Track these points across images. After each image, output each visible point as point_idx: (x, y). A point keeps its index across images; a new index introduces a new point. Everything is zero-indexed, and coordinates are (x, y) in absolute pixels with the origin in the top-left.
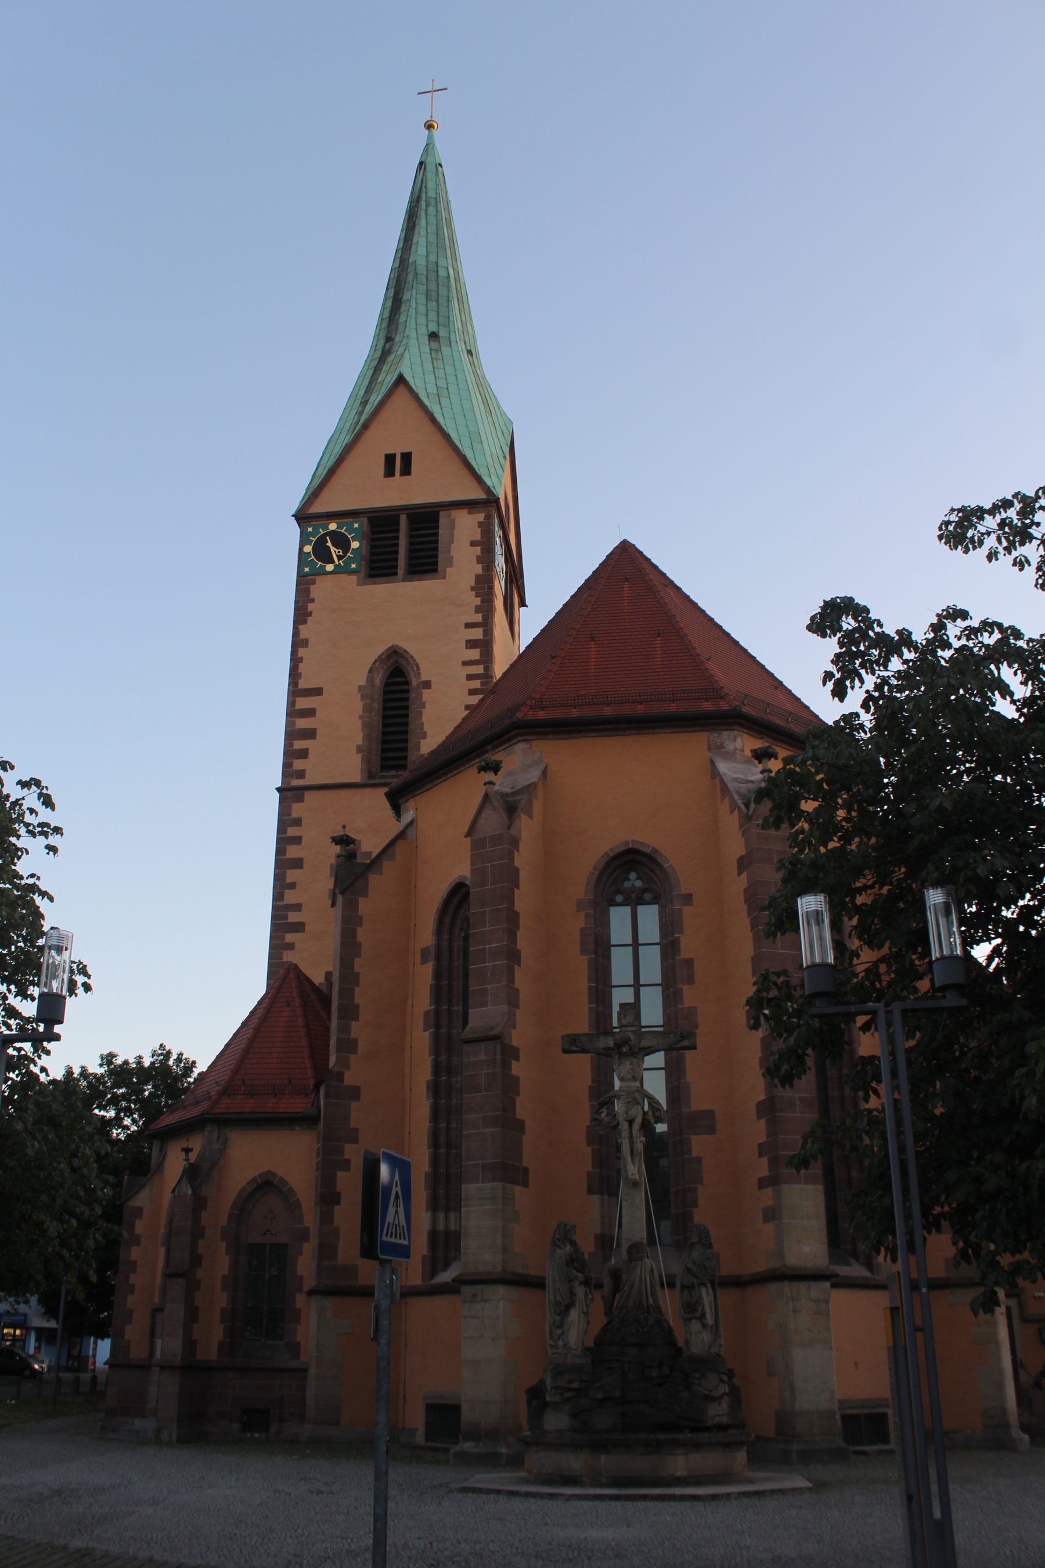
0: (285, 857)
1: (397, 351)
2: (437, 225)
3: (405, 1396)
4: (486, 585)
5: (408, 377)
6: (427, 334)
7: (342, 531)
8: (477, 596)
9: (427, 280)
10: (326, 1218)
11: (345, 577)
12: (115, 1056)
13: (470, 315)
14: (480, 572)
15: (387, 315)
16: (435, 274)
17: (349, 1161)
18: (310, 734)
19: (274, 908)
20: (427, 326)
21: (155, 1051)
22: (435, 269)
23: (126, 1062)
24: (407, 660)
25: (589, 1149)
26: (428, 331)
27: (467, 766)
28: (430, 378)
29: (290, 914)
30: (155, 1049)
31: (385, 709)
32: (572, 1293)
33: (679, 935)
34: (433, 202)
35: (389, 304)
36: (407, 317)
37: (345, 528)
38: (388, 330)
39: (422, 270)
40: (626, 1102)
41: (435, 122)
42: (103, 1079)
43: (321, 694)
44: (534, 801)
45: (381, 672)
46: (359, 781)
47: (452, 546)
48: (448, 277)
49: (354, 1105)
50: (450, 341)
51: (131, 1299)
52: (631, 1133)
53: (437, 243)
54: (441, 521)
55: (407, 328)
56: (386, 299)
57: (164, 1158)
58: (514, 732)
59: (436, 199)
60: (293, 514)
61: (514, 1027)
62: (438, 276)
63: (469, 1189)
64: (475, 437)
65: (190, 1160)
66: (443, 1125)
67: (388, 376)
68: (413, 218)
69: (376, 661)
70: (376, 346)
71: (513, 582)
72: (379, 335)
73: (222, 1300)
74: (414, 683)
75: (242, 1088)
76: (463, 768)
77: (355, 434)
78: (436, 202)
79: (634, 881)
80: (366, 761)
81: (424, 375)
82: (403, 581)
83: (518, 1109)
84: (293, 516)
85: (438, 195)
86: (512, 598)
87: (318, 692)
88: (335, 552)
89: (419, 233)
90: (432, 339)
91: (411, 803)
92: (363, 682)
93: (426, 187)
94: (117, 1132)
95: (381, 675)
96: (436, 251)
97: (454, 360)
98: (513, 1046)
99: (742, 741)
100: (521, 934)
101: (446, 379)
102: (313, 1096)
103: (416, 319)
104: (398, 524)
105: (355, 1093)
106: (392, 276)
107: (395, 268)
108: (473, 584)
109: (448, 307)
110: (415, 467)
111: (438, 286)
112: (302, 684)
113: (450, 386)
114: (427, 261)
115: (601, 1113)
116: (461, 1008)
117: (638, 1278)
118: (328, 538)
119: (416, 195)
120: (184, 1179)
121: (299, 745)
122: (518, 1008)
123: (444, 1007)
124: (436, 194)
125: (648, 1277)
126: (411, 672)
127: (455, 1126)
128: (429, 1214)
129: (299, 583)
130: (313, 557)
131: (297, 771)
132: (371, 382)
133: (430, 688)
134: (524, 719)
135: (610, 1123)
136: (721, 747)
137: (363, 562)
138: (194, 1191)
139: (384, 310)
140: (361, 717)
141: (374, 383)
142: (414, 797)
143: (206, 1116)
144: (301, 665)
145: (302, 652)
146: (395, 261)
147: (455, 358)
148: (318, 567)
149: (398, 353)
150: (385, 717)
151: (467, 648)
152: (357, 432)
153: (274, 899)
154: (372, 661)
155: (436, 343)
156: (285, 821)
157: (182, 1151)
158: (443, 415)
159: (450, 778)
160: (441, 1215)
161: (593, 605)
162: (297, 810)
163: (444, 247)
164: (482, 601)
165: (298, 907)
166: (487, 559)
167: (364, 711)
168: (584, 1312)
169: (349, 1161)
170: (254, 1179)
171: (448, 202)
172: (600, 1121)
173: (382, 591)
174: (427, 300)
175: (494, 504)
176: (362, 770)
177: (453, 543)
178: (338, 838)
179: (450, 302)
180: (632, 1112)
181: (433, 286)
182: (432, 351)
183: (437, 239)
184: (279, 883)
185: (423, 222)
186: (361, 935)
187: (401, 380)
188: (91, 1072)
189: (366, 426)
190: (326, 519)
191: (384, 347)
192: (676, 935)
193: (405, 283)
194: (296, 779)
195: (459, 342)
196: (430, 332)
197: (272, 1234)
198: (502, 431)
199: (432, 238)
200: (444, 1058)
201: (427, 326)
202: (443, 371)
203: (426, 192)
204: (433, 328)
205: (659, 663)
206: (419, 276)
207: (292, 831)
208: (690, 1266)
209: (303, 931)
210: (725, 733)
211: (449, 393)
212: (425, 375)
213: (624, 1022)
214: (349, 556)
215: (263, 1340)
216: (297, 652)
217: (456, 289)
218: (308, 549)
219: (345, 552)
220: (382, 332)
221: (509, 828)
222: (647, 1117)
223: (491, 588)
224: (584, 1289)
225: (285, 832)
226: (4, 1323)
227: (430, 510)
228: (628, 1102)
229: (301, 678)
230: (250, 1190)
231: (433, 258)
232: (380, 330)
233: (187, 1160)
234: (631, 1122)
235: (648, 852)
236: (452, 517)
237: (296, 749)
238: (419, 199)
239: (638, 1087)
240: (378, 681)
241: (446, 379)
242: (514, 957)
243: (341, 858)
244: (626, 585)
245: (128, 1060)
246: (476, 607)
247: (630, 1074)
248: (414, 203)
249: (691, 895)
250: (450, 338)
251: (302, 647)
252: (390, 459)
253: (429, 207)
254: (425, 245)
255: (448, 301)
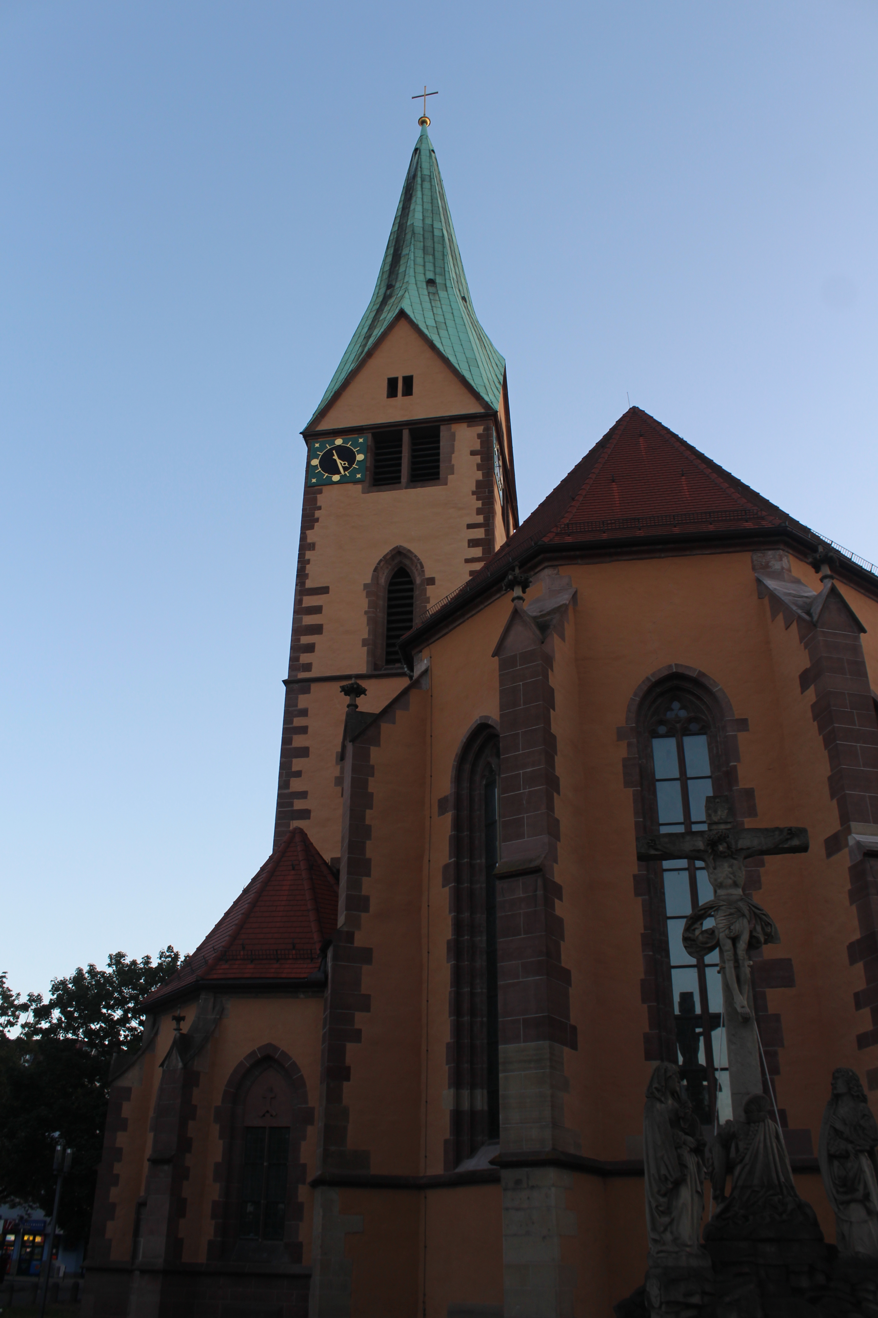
0: (291, 746)
1: (398, 294)
2: (431, 196)
3: (425, 1310)
4: (487, 490)
5: (409, 311)
6: (424, 280)
7: (348, 446)
8: (478, 499)
9: (424, 238)
10: (333, 1096)
11: (350, 486)
12: (123, 956)
13: (463, 271)
14: (481, 478)
15: (387, 268)
16: (431, 234)
17: (359, 1031)
18: (317, 629)
19: (280, 796)
20: (425, 274)
21: (163, 953)
22: (431, 229)
23: (134, 963)
24: (411, 559)
25: (645, 1006)
26: (426, 278)
27: (486, 604)
28: (429, 314)
29: (296, 802)
30: (163, 951)
31: (389, 607)
32: (683, 1166)
33: (736, 764)
34: (427, 179)
35: (389, 259)
36: (406, 267)
37: (350, 443)
38: (389, 280)
39: (419, 230)
40: (728, 913)
41: (428, 118)
42: (112, 979)
43: (327, 592)
44: (566, 624)
45: (386, 572)
46: (365, 672)
47: (453, 455)
48: (443, 236)
49: (365, 968)
50: (446, 287)
51: (114, 1191)
52: (735, 954)
53: (432, 210)
54: (441, 434)
55: (406, 276)
56: (386, 256)
57: (156, 1034)
58: (540, 557)
59: (430, 176)
60: (301, 431)
61: (556, 861)
62: (433, 235)
63: (507, 1050)
64: (472, 362)
65: (181, 1030)
66: (466, 989)
67: (389, 314)
68: (410, 191)
69: (381, 561)
70: (378, 293)
71: (508, 503)
72: (380, 285)
73: (214, 1191)
74: (418, 581)
75: (242, 953)
76: (482, 606)
77: (360, 361)
78: (431, 179)
79: (678, 711)
80: (372, 654)
81: (423, 311)
82: (406, 488)
83: (563, 957)
84: (301, 433)
85: (432, 173)
86: (507, 510)
87: (325, 590)
88: (341, 464)
89: (416, 201)
90: (430, 284)
91: (426, 652)
92: (368, 581)
93: (421, 167)
94: (125, 1033)
95: (385, 574)
96: (431, 216)
97: (450, 302)
98: (554, 882)
99: (788, 561)
100: (558, 760)
101: (443, 315)
102: (320, 960)
103: (414, 268)
104: (401, 440)
105: (366, 955)
106: (392, 238)
107: (395, 232)
108: (474, 489)
109: (443, 260)
110: (416, 389)
111: (434, 243)
112: (309, 584)
113: (447, 321)
114: (424, 224)
115: (694, 930)
116: (484, 860)
117: (762, 1145)
118: (334, 451)
119: (412, 174)
120: (174, 1052)
121: (305, 640)
122: (559, 841)
123: (466, 860)
124: (430, 172)
125: (774, 1145)
126: (415, 571)
127: (479, 990)
128: (452, 1091)
129: (306, 493)
130: (320, 469)
131: (303, 664)
132: (373, 321)
133: (435, 585)
134: (550, 543)
135: (706, 943)
136: (767, 566)
137: (368, 473)
138: (185, 1065)
139: (384, 264)
140: (366, 613)
141: (377, 321)
142: (428, 645)
143: (200, 982)
144: (308, 566)
145: (309, 555)
146: (395, 226)
147: (451, 300)
148: (324, 478)
149: (399, 295)
150: (389, 614)
151: (469, 547)
152: (361, 360)
153: (280, 788)
154: (377, 561)
155: (433, 287)
156: (292, 712)
157: (173, 1020)
158: (442, 343)
159: (468, 619)
160: (466, 1093)
161: (609, 455)
162: (303, 701)
163: (438, 213)
164: (483, 504)
165: (303, 795)
166: (486, 467)
167: (369, 607)
168: (697, 1192)
169: (359, 1031)
170: (253, 1053)
171: (441, 181)
172: (694, 940)
173: (386, 497)
174: (424, 254)
175: (493, 418)
176: (368, 662)
177: (454, 453)
178: (348, 687)
179: (445, 256)
180: (736, 927)
181: (429, 243)
182: (430, 294)
183: (432, 206)
184: (284, 771)
185: (419, 194)
186: (373, 786)
187: (402, 314)
188: (99, 971)
189: (370, 354)
190: (332, 436)
191: (385, 293)
192: (732, 764)
193: (404, 242)
194: (302, 672)
195: (454, 288)
196: (427, 279)
197: (272, 1116)
198: (497, 364)
199: (428, 206)
200: (466, 915)
201: (425, 274)
202: (440, 309)
203: (421, 171)
204: (430, 275)
205: (688, 496)
206: (416, 235)
207: (298, 722)
208: (839, 1126)
209: (309, 818)
210: (770, 552)
211: (446, 327)
212: (424, 311)
213: (715, 819)
214: (354, 467)
215: (260, 1240)
216: (304, 554)
217: (450, 248)
218: (315, 462)
219: (351, 464)
220: (383, 283)
221: (543, 643)
222: (755, 934)
223: (492, 492)
224: (696, 1159)
225: (292, 722)
226: (24, 1230)
227: (431, 424)
228: (731, 914)
229: (308, 579)
230: (248, 1065)
231: (428, 221)
232: (381, 281)
233: (178, 1029)
234: (735, 940)
235: (695, 676)
236: (452, 430)
237: (303, 644)
238: (415, 176)
239: (741, 896)
240: (383, 581)
241: (443, 315)
242: (553, 783)
243: (351, 707)
244: (641, 439)
245: (136, 960)
246: (478, 509)
247: (730, 878)
248: (410, 180)
249: (746, 720)
250: (445, 284)
251: (310, 550)
252: (392, 383)
253: (424, 183)
254: (421, 211)
255: (443, 255)
